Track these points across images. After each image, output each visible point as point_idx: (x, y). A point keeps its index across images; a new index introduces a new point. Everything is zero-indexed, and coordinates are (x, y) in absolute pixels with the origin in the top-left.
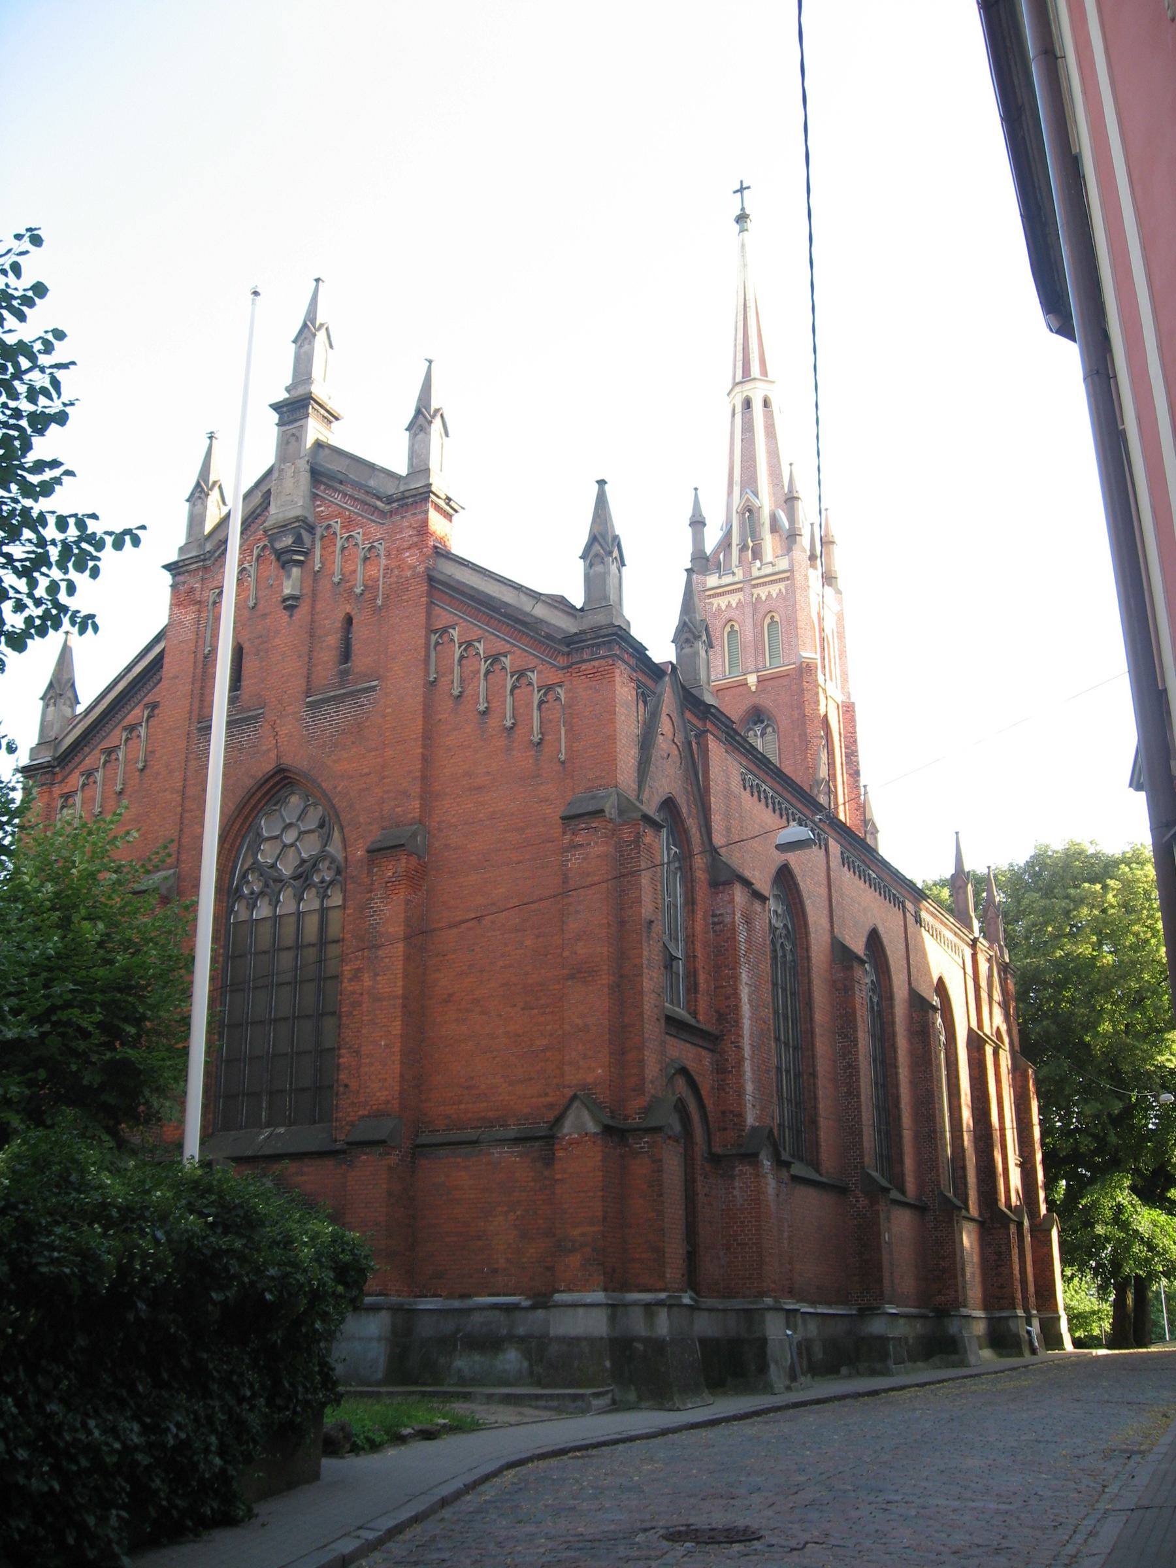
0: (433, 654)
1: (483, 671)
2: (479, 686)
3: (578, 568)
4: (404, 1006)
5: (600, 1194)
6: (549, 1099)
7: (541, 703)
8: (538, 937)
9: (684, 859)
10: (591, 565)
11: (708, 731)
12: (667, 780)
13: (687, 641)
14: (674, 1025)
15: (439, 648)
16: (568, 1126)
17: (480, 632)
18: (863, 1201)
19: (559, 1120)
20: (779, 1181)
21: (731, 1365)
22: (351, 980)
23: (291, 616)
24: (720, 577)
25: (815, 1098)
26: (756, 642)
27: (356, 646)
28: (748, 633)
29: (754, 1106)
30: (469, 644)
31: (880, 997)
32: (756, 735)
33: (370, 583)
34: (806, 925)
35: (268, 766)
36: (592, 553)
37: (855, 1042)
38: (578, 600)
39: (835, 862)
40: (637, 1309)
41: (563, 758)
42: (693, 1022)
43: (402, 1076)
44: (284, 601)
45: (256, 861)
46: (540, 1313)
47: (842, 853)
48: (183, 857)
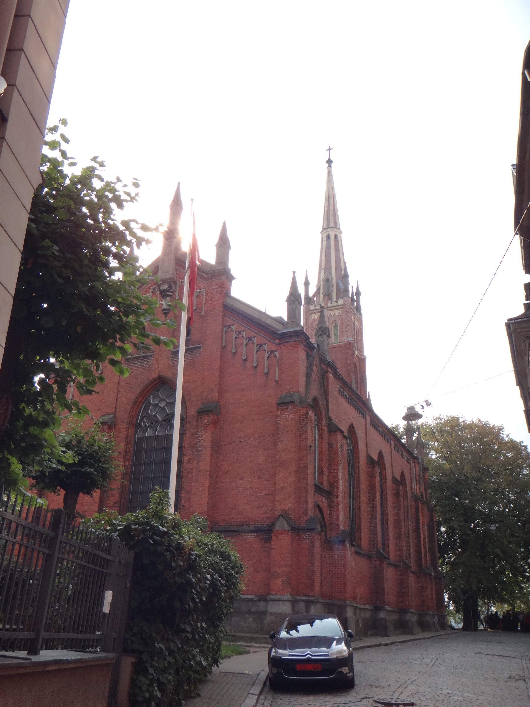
0: (224, 336)
1: (245, 343)
5: (290, 555)
6: (268, 515)
7: (268, 357)
9: (319, 421)
12: (315, 391)
13: (321, 335)
16: (277, 527)
17: (244, 328)
18: (378, 562)
19: (273, 524)
22: (187, 463)
23: (166, 317)
24: (315, 306)
25: (360, 519)
27: (193, 330)
28: (339, 323)
33: (199, 306)
34: (358, 449)
35: (155, 376)
37: (375, 497)
38: (285, 318)
39: (368, 424)
40: (302, 603)
41: (277, 379)
42: (321, 486)
44: (163, 310)
45: (148, 413)
46: (262, 603)
48: (118, 410)
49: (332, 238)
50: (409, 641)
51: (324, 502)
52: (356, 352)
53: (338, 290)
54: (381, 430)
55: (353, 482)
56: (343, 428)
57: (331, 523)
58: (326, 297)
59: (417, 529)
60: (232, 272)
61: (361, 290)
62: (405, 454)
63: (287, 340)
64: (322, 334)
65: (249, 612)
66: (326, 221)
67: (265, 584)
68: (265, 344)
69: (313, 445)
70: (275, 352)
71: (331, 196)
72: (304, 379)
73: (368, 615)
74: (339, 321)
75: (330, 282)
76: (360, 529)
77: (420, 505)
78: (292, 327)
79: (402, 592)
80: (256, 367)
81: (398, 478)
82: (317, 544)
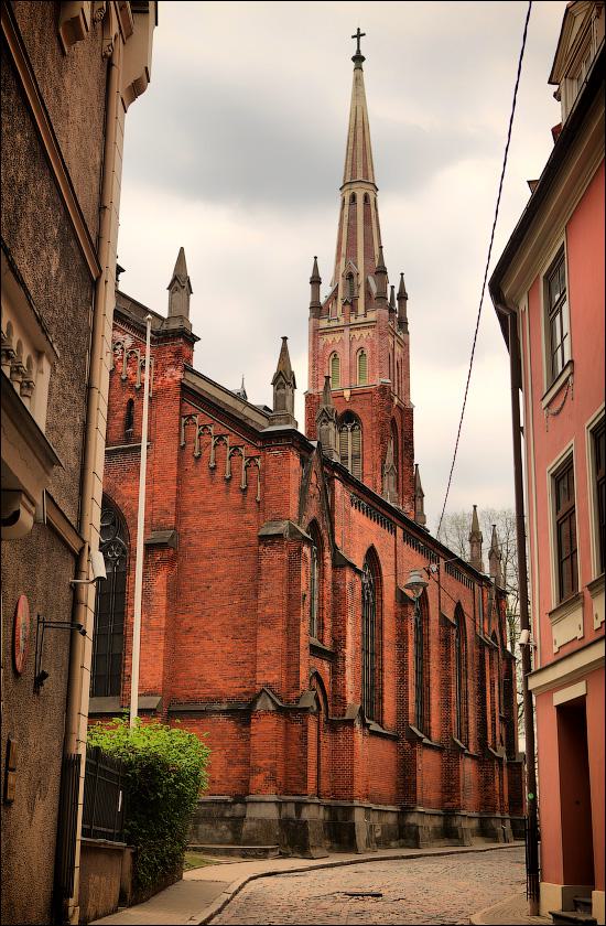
6: (244, 690)
10: (278, 389)
12: (313, 511)
14: (314, 650)
19: (254, 702)
21: (341, 837)
24: (329, 321)
26: (351, 367)
28: (367, 352)
31: (421, 618)
39: (400, 540)
41: (258, 499)
42: (321, 646)
46: (239, 806)
49: (360, 200)
50: (452, 853)
51: (325, 667)
52: (396, 400)
53: (368, 293)
56: (353, 561)
58: (348, 308)
60: (195, 331)
61: (408, 290)
65: (223, 818)
66: (349, 169)
68: (242, 447)
69: (308, 593)
71: (360, 124)
72: (297, 498)
73: (391, 819)
76: (381, 698)
77: (487, 653)
78: (281, 424)
79: (450, 786)
80: (229, 480)
81: (450, 616)
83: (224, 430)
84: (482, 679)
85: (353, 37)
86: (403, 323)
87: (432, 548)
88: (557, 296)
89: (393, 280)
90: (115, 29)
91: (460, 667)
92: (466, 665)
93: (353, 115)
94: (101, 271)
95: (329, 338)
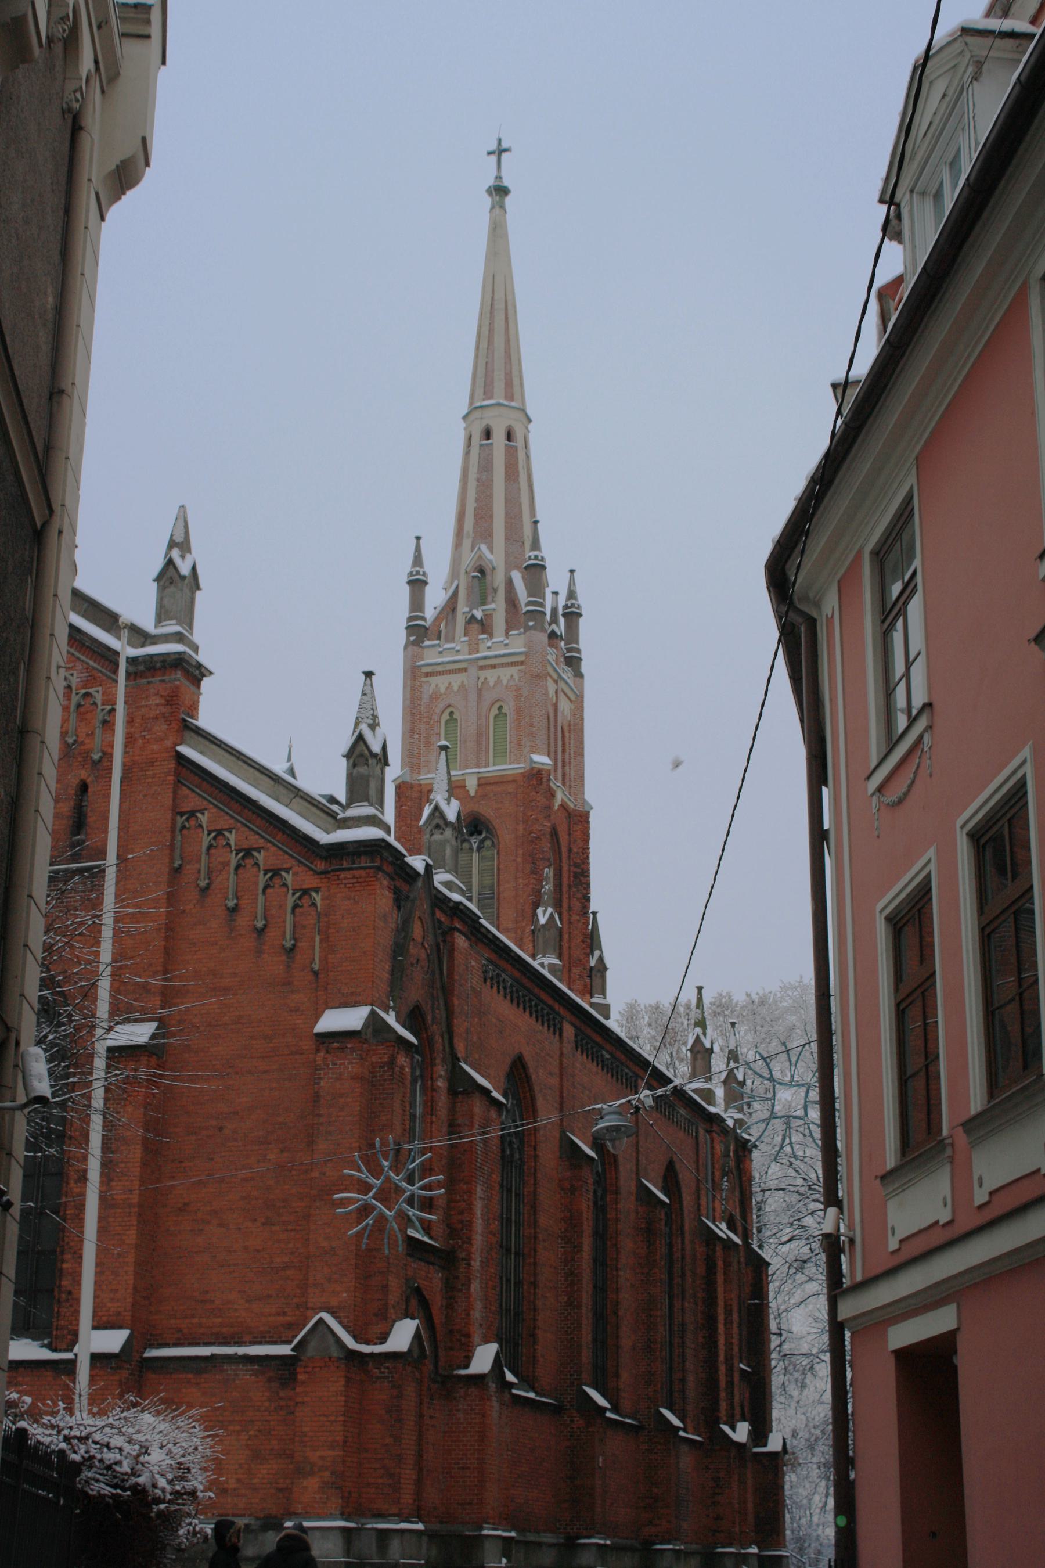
0: (179, 838)
1: (233, 864)
2: (228, 879)
3: (341, 767)
4: (140, 1215)
5: (341, 1418)
6: (288, 1318)
7: (295, 907)
8: (282, 1151)
10: (355, 765)
11: (455, 929)
13: (438, 826)
15: (185, 832)
17: (232, 821)
20: (502, 1404)
26: (479, 735)
28: (509, 709)
29: (481, 1325)
30: (220, 833)
32: (471, 849)
36: (357, 752)
39: (568, 1047)
41: (316, 967)
43: (135, 1288)
47: (576, 1036)
52: (559, 796)
53: (512, 602)
54: (607, 1056)
55: (518, 1212)
57: (451, 1331)
59: (710, 1320)
61: (583, 600)
62: (682, 1112)
63: (345, 865)
64: (441, 823)
67: (280, 1490)
68: (287, 871)
70: (314, 894)
71: (500, 306)
74: (512, 704)
75: (488, 577)
80: (261, 932)
82: (410, 1390)
83: (254, 840)
84: (711, 1300)
85: (489, 153)
86: (573, 662)
87: (623, 1063)
88: (896, 588)
89: (556, 580)
90: (87, 64)
91: (671, 1278)
92: (683, 1275)
93: (489, 289)
94: (51, 511)
95: (440, 683)
